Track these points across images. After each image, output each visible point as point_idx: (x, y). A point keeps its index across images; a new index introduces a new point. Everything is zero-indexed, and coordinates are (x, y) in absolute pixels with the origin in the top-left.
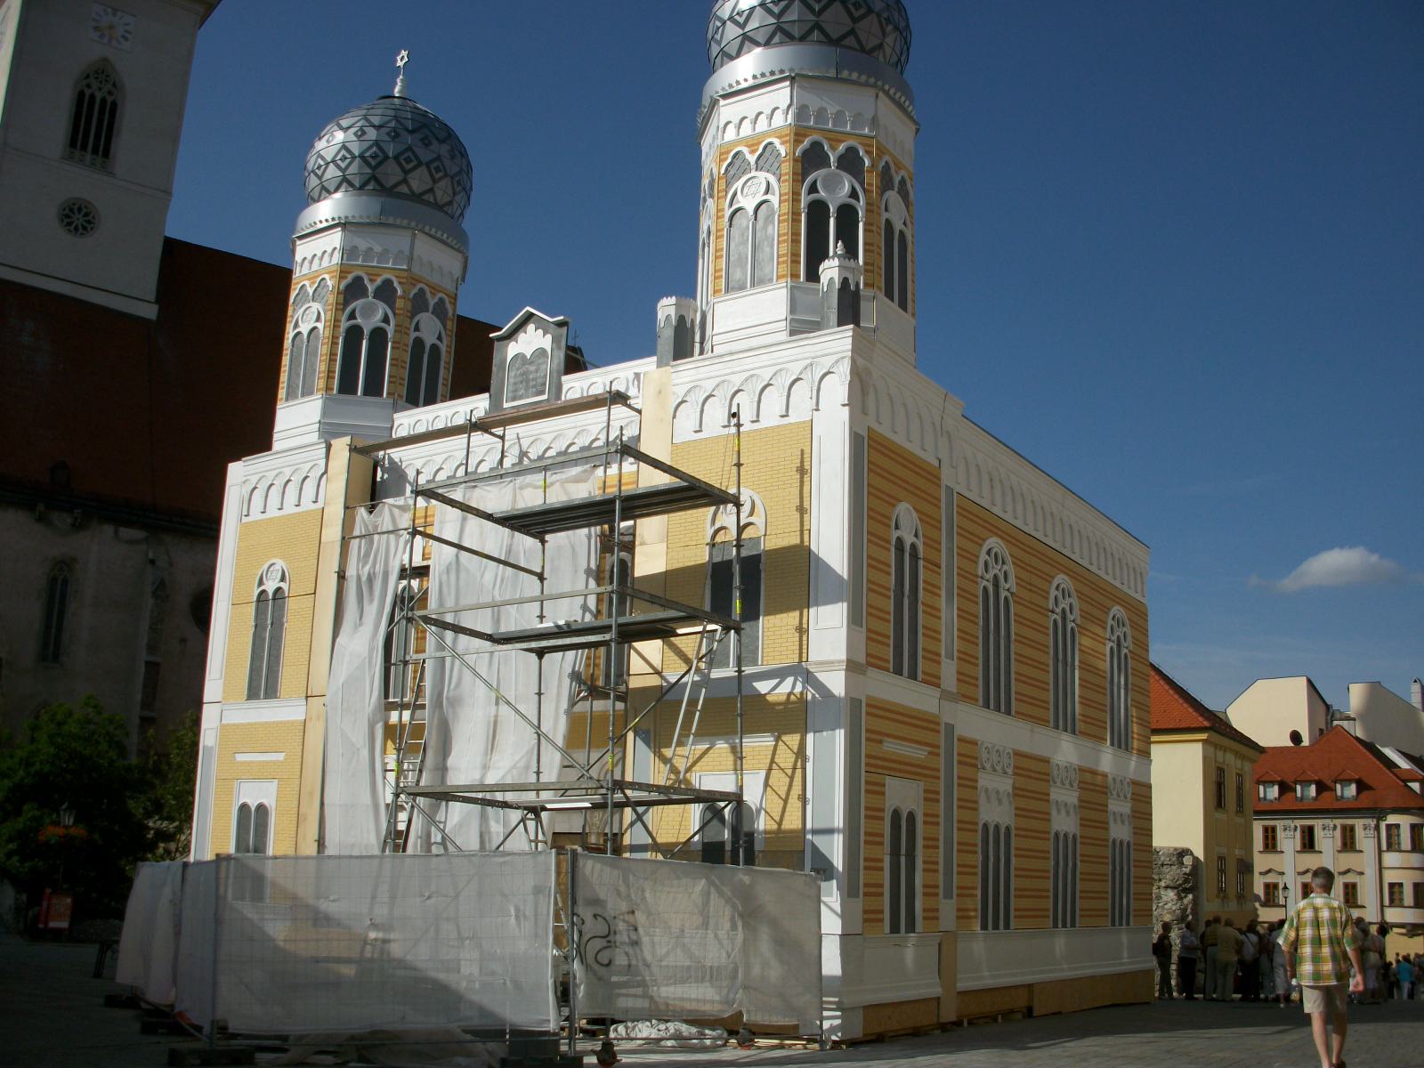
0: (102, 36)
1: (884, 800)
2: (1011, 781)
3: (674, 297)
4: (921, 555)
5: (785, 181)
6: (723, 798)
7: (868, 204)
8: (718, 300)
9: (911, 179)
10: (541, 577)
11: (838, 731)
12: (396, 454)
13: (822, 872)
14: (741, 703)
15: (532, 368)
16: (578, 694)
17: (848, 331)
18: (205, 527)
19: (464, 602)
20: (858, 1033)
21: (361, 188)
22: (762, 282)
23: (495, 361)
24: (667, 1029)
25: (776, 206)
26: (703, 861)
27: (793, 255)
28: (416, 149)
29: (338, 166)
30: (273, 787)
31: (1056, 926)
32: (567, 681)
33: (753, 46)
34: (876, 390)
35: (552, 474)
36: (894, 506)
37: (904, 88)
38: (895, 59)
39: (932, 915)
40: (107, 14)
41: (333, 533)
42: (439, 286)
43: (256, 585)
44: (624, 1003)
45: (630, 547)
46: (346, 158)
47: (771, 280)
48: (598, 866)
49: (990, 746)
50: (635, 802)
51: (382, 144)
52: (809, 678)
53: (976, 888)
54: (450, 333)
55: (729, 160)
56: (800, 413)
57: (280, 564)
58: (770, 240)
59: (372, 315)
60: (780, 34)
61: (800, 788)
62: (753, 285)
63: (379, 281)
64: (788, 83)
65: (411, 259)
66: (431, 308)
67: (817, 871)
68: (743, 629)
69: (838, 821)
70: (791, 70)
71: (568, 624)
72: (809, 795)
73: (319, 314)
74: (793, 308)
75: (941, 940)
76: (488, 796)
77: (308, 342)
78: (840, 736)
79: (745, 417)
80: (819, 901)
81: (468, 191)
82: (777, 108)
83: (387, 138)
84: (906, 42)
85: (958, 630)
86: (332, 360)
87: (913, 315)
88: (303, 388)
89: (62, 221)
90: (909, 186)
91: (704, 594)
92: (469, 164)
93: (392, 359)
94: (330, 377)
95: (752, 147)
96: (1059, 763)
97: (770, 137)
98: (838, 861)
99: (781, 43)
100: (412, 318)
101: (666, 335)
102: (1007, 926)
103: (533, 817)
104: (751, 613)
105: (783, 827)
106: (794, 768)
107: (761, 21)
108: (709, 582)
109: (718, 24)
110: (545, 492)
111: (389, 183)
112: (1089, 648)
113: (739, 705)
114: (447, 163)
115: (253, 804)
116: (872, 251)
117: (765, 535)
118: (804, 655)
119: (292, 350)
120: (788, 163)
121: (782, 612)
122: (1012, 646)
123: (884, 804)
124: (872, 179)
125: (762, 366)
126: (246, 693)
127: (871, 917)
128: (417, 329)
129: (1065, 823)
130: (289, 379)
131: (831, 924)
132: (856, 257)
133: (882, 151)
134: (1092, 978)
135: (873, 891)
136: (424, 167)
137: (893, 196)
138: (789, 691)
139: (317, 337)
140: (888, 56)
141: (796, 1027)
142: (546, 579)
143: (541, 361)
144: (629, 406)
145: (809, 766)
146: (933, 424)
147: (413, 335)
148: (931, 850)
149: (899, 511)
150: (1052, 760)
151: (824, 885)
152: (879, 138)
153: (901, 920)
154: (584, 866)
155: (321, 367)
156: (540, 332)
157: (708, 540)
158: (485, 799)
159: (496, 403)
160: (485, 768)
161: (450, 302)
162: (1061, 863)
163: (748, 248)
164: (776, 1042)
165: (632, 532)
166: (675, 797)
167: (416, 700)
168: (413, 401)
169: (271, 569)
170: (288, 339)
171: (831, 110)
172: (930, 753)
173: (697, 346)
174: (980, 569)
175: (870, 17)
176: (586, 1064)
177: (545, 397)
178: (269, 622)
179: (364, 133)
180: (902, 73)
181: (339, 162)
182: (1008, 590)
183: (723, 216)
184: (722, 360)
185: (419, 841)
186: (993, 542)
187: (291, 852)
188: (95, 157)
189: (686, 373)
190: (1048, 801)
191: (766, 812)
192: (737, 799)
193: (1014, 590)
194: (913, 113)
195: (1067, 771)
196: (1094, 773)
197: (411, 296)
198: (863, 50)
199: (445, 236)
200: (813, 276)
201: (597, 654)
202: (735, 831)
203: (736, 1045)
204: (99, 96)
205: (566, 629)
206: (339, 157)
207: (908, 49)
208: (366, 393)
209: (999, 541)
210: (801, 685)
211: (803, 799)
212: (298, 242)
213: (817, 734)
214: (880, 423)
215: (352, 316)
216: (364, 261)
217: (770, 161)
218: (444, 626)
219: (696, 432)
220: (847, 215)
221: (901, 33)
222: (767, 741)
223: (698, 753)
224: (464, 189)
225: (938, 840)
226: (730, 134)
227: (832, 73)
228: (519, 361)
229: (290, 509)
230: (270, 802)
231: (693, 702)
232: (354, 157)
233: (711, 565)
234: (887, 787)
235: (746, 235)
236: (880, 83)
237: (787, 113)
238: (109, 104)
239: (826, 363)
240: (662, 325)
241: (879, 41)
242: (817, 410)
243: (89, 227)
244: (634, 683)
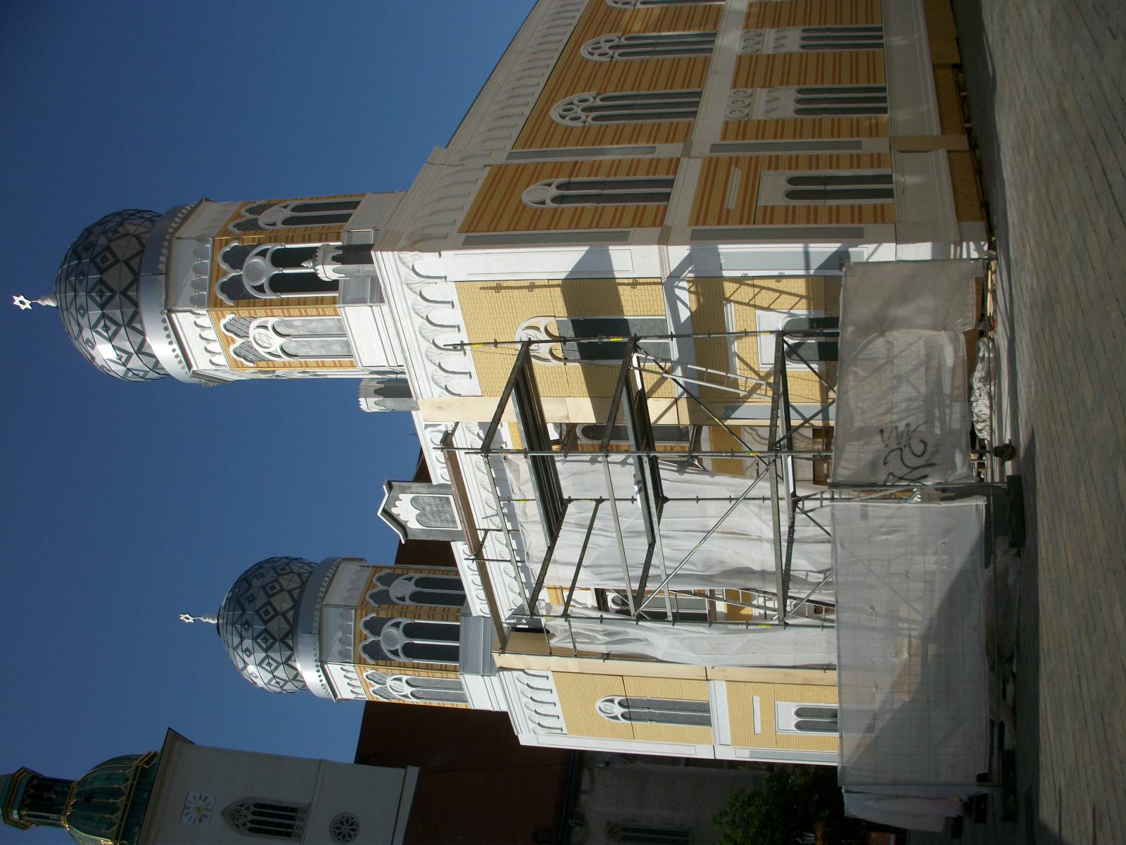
0: (206, 816)
1: (778, 206)
2: (758, 89)
3: (360, 399)
4: (565, 180)
5: (255, 313)
6: (781, 349)
7: (270, 241)
8: (359, 363)
9: (249, 203)
10: (600, 501)
11: (720, 251)
12: (505, 614)
13: (842, 262)
14: (700, 335)
15: (428, 508)
16: (697, 467)
17: (376, 255)
18: (575, 762)
19: (619, 561)
20: (980, 226)
21: (291, 649)
22: (341, 328)
23: (424, 538)
24: (979, 389)
25: (276, 319)
26: (837, 360)
27: (316, 304)
28: (257, 607)
29: (276, 669)
30: (781, 705)
31: (881, 45)
32: (686, 476)
33: (145, 346)
34: (426, 227)
35: (514, 493)
36: (525, 206)
37: (173, 213)
38: (148, 223)
39: (876, 160)
40: (189, 813)
41: (572, 664)
42: (367, 581)
43: (617, 721)
44: (956, 422)
45: (572, 427)
46: (269, 663)
47: (339, 321)
48: (843, 463)
49: (728, 110)
50: (787, 431)
51: (255, 635)
52: (675, 276)
53: (852, 119)
54: (405, 571)
55: (242, 360)
56: (450, 292)
57: (599, 703)
58: (306, 323)
59: (394, 637)
60: (132, 323)
61: (770, 280)
62: (344, 335)
63: (365, 632)
64: (173, 315)
65: (346, 607)
66: (385, 588)
67: (841, 266)
68: (635, 334)
69: (798, 247)
70: (162, 313)
71: (637, 483)
72: (776, 273)
73: (395, 679)
74: (360, 301)
75: (898, 151)
76: (785, 537)
77: (418, 687)
78: (724, 249)
79: (455, 338)
80: (867, 263)
81: (290, 561)
82: (195, 323)
83: (250, 631)
84: (133, 215)
85: (630, 143)
86: (432, 668)
87: (363, 195)
88: (456, 689)
89: (348, 841)
90: (254, 205)
91: (608, 366)
92: (267, 561)
93: (429, 619)
94: (446, 669)
95: (229, 342)
96: (742, 46)
97: (219, 328)
98: (832, 247)
99: (141, 322)
100: (394, 604)
101: (391, 404)
102: (883, 89)
103: (801, 502)
104: (621, 326)
105: (804, 294)
106: (754, 286)
107: (124, 340)
108: (597, 362)
109: (130, 374)
110: (528, 500)
111: (286, 627)
112: (642, 25)
113: (701, 336)
114: (267, 580)
115: (796, 719)
116: (310, 235)
117: (555, 316)
118: (656, 280)
119: (426, 699)
120: (240, 311)
121: (619, 300)
122: (642, 93)
123: (781, 206)
124: (249, 238)
125: (411, 326)
126: (706, 727)
127: (880, 216)
128: (403, 599)
129: (793, 40)
130: (450, 700)
131: (887, 252)
132: (316, 248)
133: (225, 232)
134: (926, 11)
135: (857, 215)
136: (271, 599)
137: (262, 220)
138: (687, 293)
139: (414, 680)
140: (146, 230)
141: (977, 279)
142: (601, 497)
143: (422, 502)
144: (454, 431)
145: (751, 273)
146: (454, 173)
147: (408, 602)
148: (820, 161)
149: (530, 201)
150: (739, 54)
151: (853, 259)
152: (214, 235)
153: (880, 188)
154: (842, 476)
155: (438, 675)
156: (397, 503)
157: (562, 364)
158: (787, 542)
159: (458, 536)
160: (760, 539)
161: (380, 572)
162: (827, 42)
163: (315, 341)
164: (989, 296)
165: (559, 426)
166: (781, 390)
167: (707, 596)
168: (461, 600)
169: (604, 710)
170: (417, 702)
171: (193, 277)
172: (736, 165)
173: (399, 376)
174: (578, 124)
175: (113, 247)
176: (1013, 472)
177: (451, 497)
178: (647, 710)
179: (247, 650)
180: (160, 216)
181: (272, 668)
182: (595, 98)
183: (289, 362)
184: (409, 359)
185: (823, 592)
186: (554, 114)
187: (836, 690)
188: (297, 818)
189: (421, 385)
190: (774, 55)
191: (791, 309)
192: (780, 335)
193: (594, 93)
194: (192, 205)
195: (748, 39)
196: (749, 15)
197: (376, 605)
198: (141, 252)
199: (328, 574)
200: (333, 286)
201: (663, 450)
202: (808, 335)
203: (992, 332)
204: (251, 817)
205: (641, 485)
206: (269, 669)
207: (139, 212)
208: (457, 639)
209: (582, 47)
210: (681, 283)
211: (779, 278)
212: (339, 697)
213: (723, 268)
214: (455, 221)
215: (395, 653)
216: (350, 645)
217: (240, 326)
218: (644, 579)
219: (471, 377)
220: (280, 259)
221: (126, 219)
222: (731, 311)
223: (743, 366)
224: (288, 564)
225: (811, 156)
226: (221, 360)
227: (162, 278)
228: (423, 519)
229: (554, 697)
230: (794, 707)
231: (700, 375)
232: (268, 657)
233: (583, 361)
234: (766, 204)
235: (303, 343)
236: (168, 237)
237: (199, 314)
238: (256, 809)
239: (405, 272)
240: (384, 408)
241: (133, 238)
242: (446, 278)
243: (351, 821)
244: (685, 420)
